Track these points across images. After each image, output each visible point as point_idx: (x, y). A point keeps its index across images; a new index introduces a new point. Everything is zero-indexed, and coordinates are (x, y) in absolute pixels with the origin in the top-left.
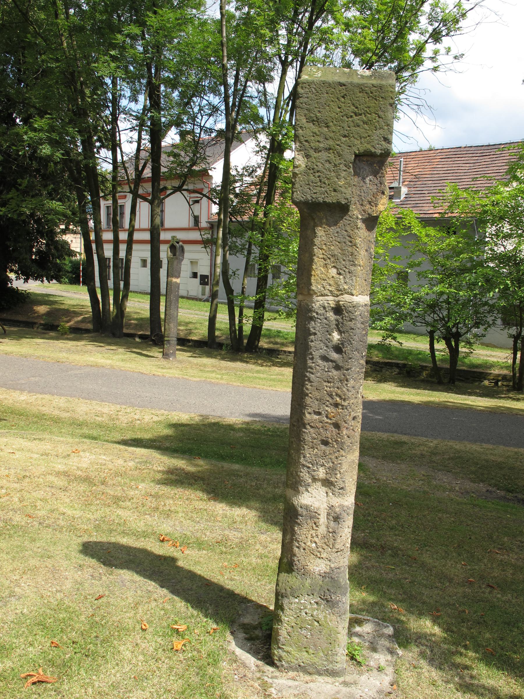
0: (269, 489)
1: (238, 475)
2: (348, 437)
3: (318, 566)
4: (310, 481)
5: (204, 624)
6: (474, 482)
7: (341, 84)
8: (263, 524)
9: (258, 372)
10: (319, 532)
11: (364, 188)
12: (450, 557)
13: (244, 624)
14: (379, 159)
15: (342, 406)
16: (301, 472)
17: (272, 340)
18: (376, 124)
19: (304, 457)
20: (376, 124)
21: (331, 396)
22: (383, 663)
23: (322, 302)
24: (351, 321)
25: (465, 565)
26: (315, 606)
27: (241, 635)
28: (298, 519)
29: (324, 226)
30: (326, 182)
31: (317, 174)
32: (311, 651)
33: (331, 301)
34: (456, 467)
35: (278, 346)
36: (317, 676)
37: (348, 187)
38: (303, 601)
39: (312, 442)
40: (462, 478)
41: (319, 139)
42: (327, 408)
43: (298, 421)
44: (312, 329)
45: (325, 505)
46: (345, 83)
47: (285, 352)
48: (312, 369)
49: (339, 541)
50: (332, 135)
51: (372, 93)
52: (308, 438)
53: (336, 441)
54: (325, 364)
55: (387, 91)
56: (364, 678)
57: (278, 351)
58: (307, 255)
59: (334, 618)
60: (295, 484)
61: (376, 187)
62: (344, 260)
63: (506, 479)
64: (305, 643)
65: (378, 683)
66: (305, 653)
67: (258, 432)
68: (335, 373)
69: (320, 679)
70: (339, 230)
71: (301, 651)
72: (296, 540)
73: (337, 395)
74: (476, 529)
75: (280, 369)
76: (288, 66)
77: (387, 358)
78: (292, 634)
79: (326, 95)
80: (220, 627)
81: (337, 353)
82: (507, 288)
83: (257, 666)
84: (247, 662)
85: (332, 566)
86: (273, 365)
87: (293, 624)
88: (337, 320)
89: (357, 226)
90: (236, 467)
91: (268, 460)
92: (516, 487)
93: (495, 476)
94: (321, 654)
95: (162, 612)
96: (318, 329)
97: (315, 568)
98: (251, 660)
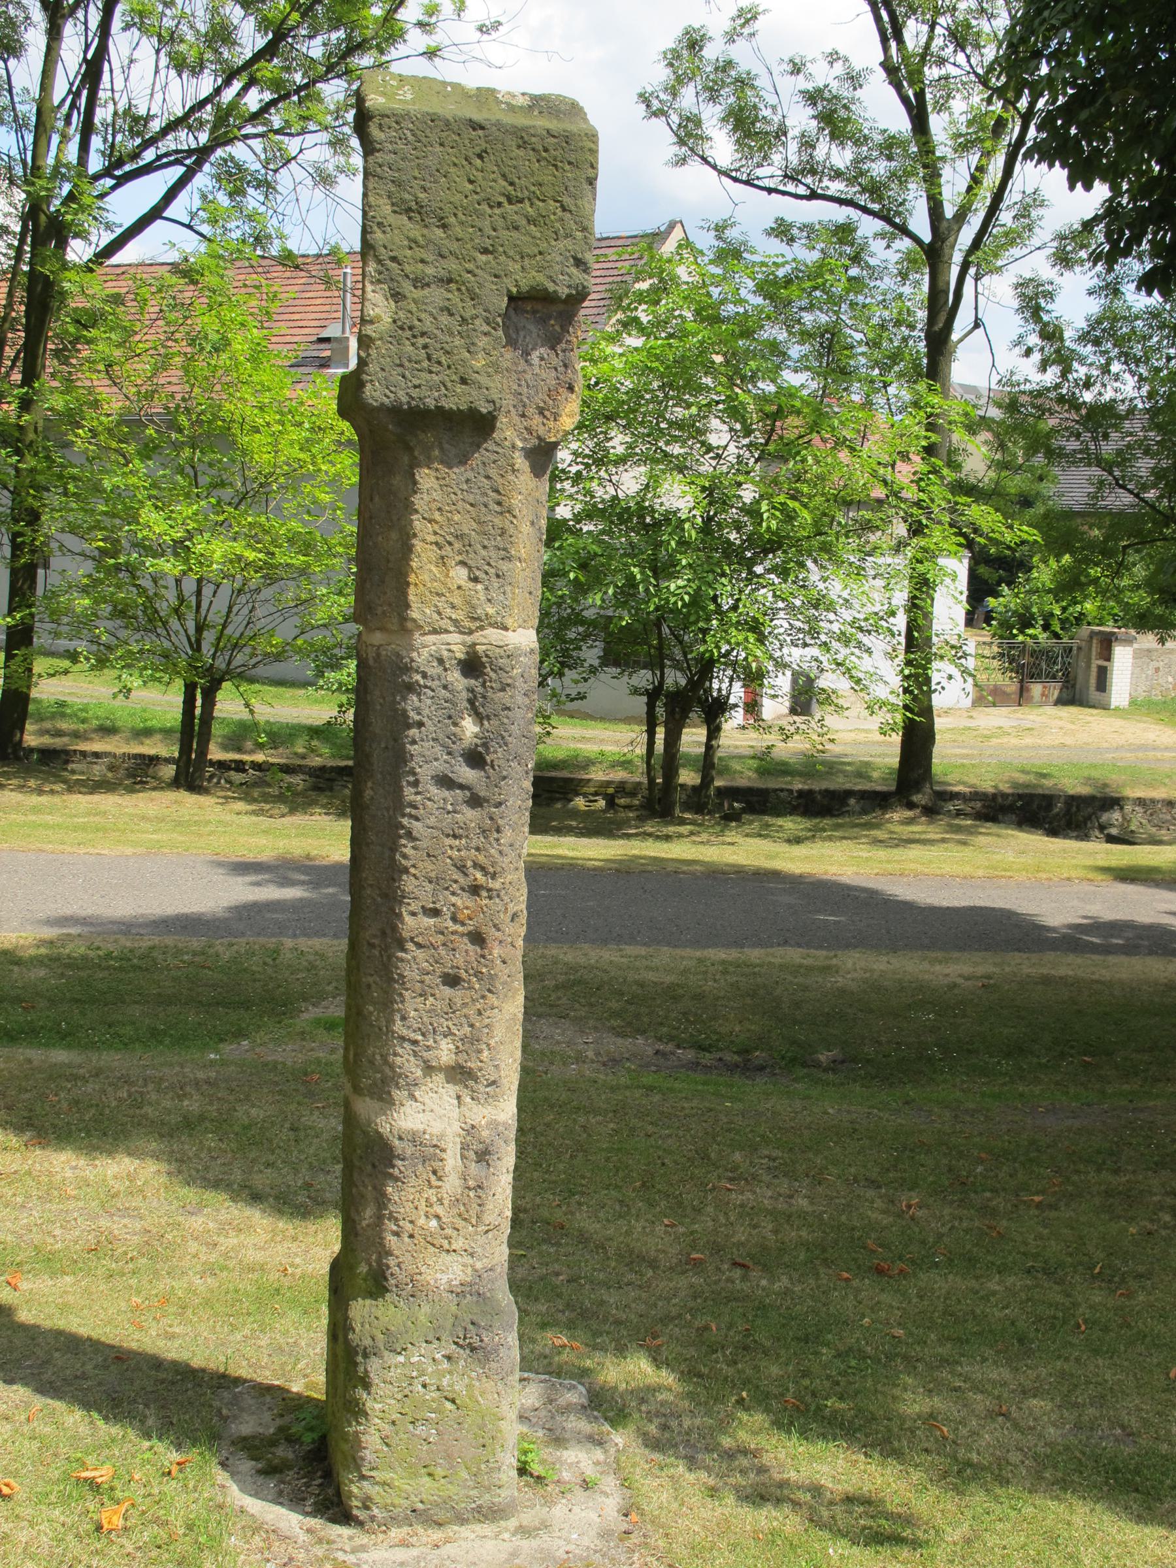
0: (167, 1103)
1: (75, 1078)
2: (504, 962)
3: (445, 1272)
4: (419, 1073)
5: (148, 1455)
6: (623, 1035)
7: (475, 126)
8: (186, 1190)
9: (35, 810)
10: (443, 1191)
11: (528, 377)
12: (633, 1211)
13: (245, 1439)
14: (561, 307)
15: (489, 890)
16: (395, 1055)
17: (48, 725)
18: (557, 225)
19: (403, 1018)
20: (557, 225)
21: (462, 869)
22: (590, 1472)
23: (434, 647)
24: (503, 690)
25: (672, 1226)
26: (445, 1365)
27: (247, 1466)
28: (393, 1166)
29: (436, 465)
30: (443, 359)
31: (421, 341)
32: (439, 1472)
33: (455, 644)
34: (577, 1006)
35: (66, 739)
36: (456, 1528)
37: (493, 373)
38: (415, 1359)
39: (422, 982)
40: (596, 1028)
41: (424, 256)
42: (453, 899)
43: (384, 933)
44: (412, 714)
45: (456, 1127)
46: (484, 123)
47: (84, 754)
48: (416, 808)
49: (490, 1206)
50: (455, 246)
51: (546, 150)
52: (410, 973)
53: (478, 974)
54: (446, 793)
55: (582, 148)
56: (559, 1510)
57: (66, 752)
58: (394, 535)
59: (489, 1385)
60: (383, 1086)
61: (554, 374)
62: (485, 547)
63: (692, 1023)
64: (424, 1455)
65: (593, 1516)
66: (427, 1479)
67: (82, 964)
68: (470, 815)
69: (465, 1531)
70: (470, 475)
71: (416, 1475)
72: (391, 1217)
73: (476, 865)
74: (670, 1141)
75: (89, 798)
76: (65, 18)
77: (342, 758)
78: (393, 1442)
79: (438, 149)
80: (194, 1454)
81: (473, 768)
82: (631, 581)
83: (309, 1531)
84: (282, 1525)
85: (479, 1265)
86: (70, 790)
87: (396, 1416)
88: (471, 690)
89: (513, 465)
90: (60, 1056)
91: (128, 1030)
92: (715, 1037)
93: (666, 1017)
94: (464, 1474)
95: (36, 1445)
96: (426, 712)
97: (439, 1276)
98: (291, 1521)
